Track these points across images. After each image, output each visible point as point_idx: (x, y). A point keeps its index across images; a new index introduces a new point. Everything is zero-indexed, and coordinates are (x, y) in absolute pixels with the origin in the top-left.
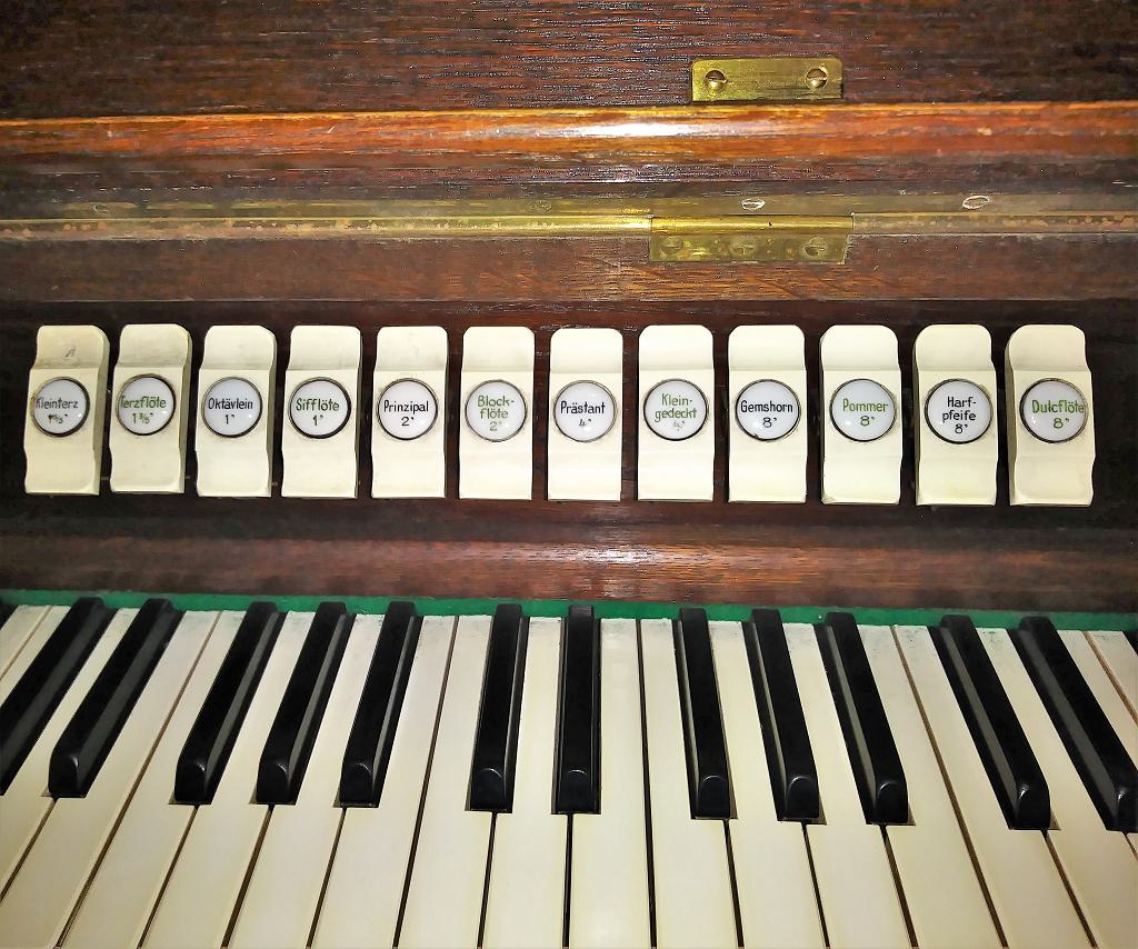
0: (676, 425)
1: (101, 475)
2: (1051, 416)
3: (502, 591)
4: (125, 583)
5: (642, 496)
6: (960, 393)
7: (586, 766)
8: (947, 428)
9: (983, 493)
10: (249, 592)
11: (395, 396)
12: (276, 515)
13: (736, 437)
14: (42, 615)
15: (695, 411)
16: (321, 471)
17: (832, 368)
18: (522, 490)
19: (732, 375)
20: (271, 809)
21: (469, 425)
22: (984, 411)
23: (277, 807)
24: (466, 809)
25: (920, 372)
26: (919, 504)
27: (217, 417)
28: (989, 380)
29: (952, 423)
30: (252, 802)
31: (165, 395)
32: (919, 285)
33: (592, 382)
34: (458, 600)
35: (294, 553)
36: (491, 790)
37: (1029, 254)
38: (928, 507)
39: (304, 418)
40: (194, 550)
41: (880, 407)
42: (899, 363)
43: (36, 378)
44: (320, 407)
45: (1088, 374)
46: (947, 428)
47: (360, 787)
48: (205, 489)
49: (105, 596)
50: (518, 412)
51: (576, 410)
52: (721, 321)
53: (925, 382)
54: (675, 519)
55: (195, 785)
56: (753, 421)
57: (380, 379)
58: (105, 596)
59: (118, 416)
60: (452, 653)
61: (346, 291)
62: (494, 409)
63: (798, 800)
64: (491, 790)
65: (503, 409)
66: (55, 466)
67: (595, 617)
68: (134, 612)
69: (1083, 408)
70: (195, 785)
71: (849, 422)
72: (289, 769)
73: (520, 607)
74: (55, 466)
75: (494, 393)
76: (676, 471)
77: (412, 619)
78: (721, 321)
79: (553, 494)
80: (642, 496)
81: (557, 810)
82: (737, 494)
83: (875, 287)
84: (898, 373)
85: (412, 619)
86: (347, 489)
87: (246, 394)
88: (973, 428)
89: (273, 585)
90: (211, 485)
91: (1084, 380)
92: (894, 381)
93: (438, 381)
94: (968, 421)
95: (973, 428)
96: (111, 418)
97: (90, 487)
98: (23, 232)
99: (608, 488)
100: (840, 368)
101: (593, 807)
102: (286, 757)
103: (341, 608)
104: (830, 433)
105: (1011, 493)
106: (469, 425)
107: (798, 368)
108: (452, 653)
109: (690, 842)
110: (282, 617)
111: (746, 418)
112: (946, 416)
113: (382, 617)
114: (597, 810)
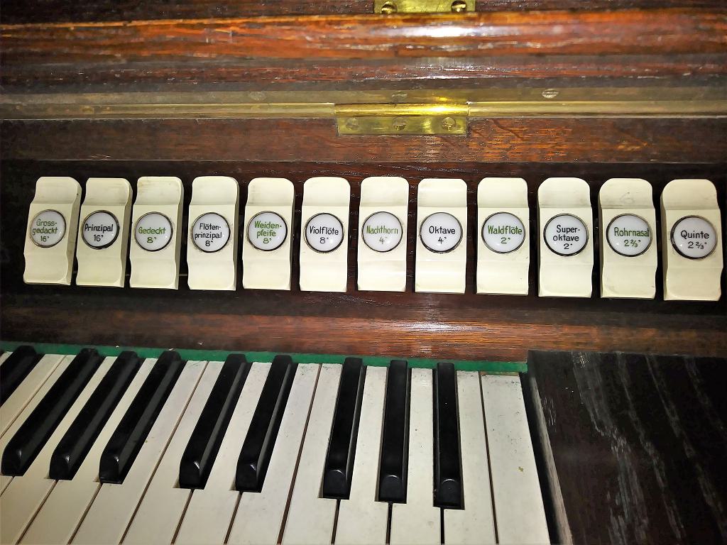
0: (440, 240)
1: (180, 273)
2: (500, 236)
3: (351, 348)
4: (150, 343)
5: (480, 290)
6: (566, 223)
7: (399, 474)
8: (558, 246)
9: (520, 287)
10: (226, 348)
11: (620, 224)
12: (243, 299)
13: (420, 250)
14: (61, 359)
15: (164, 229)
16: (267, 273)
17: (546, 206)
18: (340, 286)
19: (480, 210)
20: (192, 491)
21: (250, 242)
22: (584, 234)
23: (245, 494)
24: (376, 501)
25: (541, 209)
26: (666, 299)
27: (314, 239)
28: (587, 214)
29: (262, 238)
30: (176, 487)
31: (166, 225)
32: (596, 153)
33: (567, 215)
34: (320, 355)
35: (260, 324)
36: (336, 484)
37: (622, 128)
38: (606, 299)
39: (432, 240)
40: (184, 322)
41: (517, 231)
42: (719, 204)
43: (34, 209)
44: (511, 232)
45: (718, 212)
46: (558, 246)
47: (250, 477)
48: (195, 283)
49: (139, 351)
50: (281, 234)
51: (499, 231)
52: (473, 175)
53: (544, 215)
54: (502, 304)
55: (193, 474)
56: (494, 240)
57: (364, 213)
58: (139, 351)
59: (136, 238)
60: (315, 387)
61: (398, 154)
62: (211, 232)
63: (392, 488)
64: (336, 484)
65: (274, 230)
66: (43, 266)
67: (408, 366)
68: (155, 360)
69: (648, 233)
70: (193, 474)
71: (314, 239)
72: (256, 467)
73: (361, 360)
74: (43, 266)
75: (264, 219)
76: (441, 274)
77: (289, 366)
78: (473, 175)
79: (481, 290)
80: (480, 290)
81: (380, 498)
82: (607, 293)
83: (518, 151)
84: (654, 210)
85: (289, 366)
86: (399, 285)
87: (334, 224)
88: (216, 244)
89: (181, 342)
90: (197, 282)
91: (715, 216)
92: (524, 214)
93: (344, 215)
94: (272, 237)
95: (575, 246)
96: (76, 235)
97: (230, 286)
98: (723, 107)
99: (338, 283)
100: (611, 207)
101: (458, 504)
102: (255, 461)
103: (242, 358)
104: (246, 244)
105: (664, 290)
106: (250, 242)
107: (522, 206)
108: (315, 387)
109: (312, 509)
110: (183, 365)
111: (368, 237)
112: (555, 238)
113: (269, 365)
114: (405, 503)
